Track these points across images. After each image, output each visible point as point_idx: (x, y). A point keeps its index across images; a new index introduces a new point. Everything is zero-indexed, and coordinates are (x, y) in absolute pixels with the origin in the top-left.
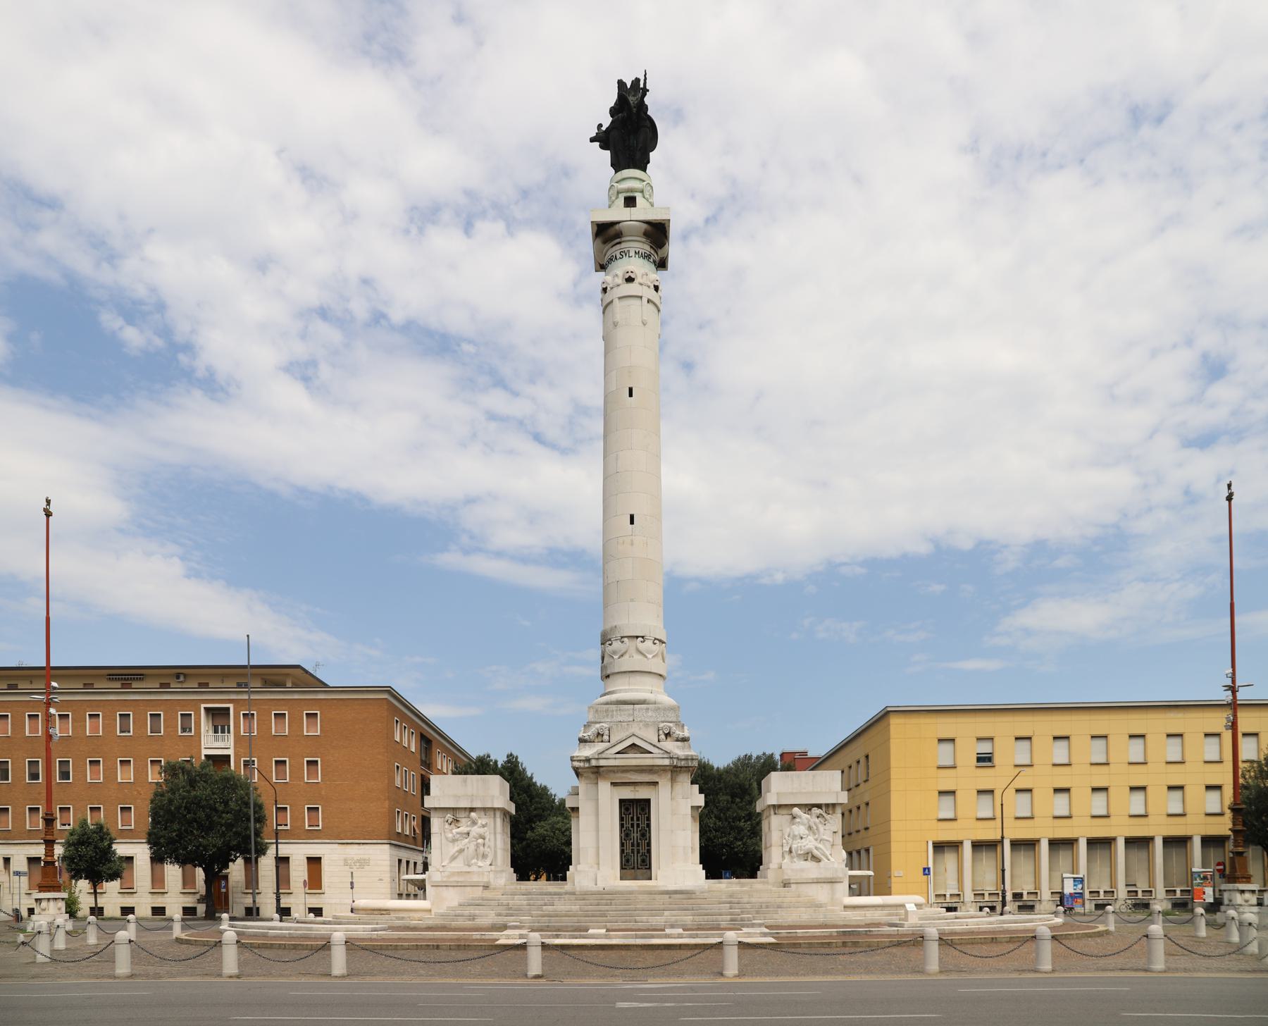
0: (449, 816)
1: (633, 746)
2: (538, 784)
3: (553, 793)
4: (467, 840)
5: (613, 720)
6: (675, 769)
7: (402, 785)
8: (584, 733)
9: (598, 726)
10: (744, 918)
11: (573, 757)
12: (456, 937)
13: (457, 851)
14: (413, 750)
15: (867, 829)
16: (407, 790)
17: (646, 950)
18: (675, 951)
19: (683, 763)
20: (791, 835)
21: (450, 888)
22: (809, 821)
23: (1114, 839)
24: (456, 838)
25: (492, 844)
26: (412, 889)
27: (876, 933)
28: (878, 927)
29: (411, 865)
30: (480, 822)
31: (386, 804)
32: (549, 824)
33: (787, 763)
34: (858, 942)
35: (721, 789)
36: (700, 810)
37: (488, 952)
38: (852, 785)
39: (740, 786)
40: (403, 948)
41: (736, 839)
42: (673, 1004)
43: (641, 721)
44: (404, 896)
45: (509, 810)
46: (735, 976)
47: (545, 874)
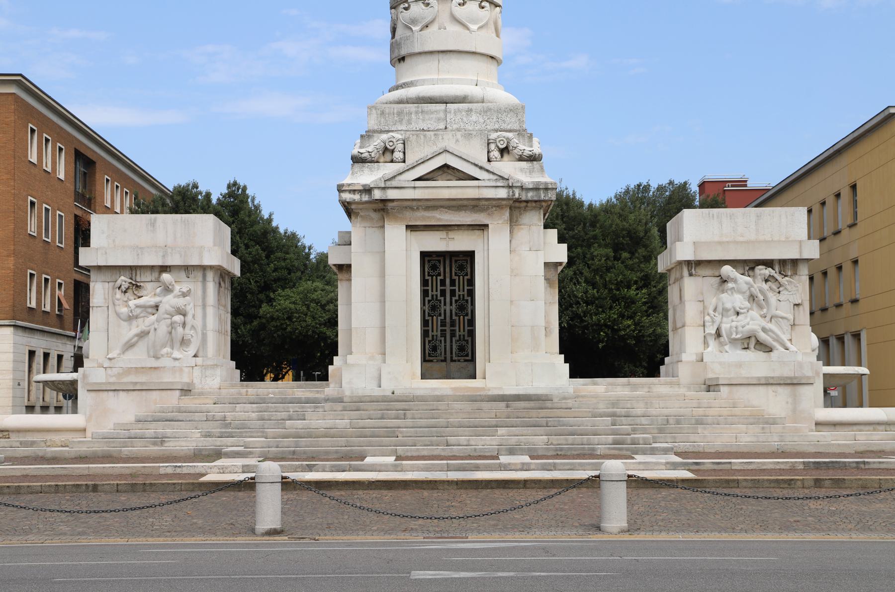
0: (123, 280)
1: (445, 169)
2: (282, 231)
3: (307, 245)
4: (153, 318)
5: (410, 127)
6: (517, 204)
7: (40, 233)
8: (361, 147)
9: (384, 137)
10: (638, 438)
11: (343, 185)
12: (128, 472)
13: (137, 335)
14: (62, 176)
15: (855, 301)
16: (49, 240)
17: (466, 488)
18: (515, 490)
19: (530, 195)
20: (720, 309)
21: (121, 393)
22: (750, 286)
24: (135, 314)
25: (198, 323)
26: (52, 397)
27: (875, 466)
28: (880, 457)
29: (53, 361)
30: (177, 288)
31: (11, 262)
32: (299, 294)
33: (711, 197)
34: (844, 479)
35: (595, 237)
36: (560, 268)
37: (185, 495)
38: (827, 232)
39: (629, 232)
40: (31, 491)
41: (622, 316)
42: (512, 574)
43: (458, 130)
44: (38, 409)
45: (229, 269)
46: (623, 531)
47: (290, 373)
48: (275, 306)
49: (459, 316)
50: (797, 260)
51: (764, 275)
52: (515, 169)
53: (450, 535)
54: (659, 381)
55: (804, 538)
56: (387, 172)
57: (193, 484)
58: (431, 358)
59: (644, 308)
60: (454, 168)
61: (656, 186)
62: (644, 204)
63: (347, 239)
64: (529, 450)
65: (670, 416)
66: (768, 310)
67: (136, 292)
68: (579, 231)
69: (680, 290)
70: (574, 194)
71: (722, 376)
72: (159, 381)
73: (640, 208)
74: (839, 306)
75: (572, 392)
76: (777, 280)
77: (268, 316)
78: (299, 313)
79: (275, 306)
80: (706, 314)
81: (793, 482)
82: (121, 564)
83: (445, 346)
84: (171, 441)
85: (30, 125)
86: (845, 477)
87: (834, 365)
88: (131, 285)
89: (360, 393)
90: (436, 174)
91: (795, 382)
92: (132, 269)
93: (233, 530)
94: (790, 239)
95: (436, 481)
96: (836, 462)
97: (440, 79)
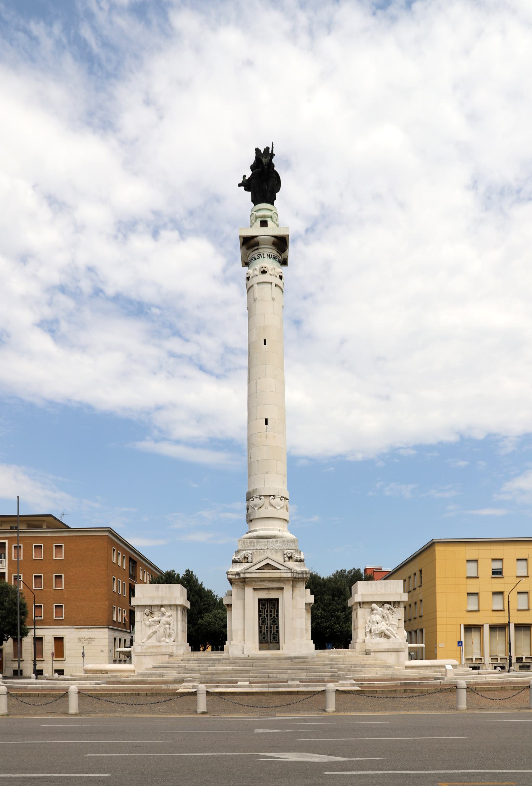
0: (147, 611)
1: (268, 565)
2: (206, 589)
3: (216, 595)
5: (254, 548)
6: (295, 579)
7: (117, 591)
8: (235, 556)
9: (244, 552)
10: (340, 674)
11: (229, 572)
12: (150, 688)
13: (152, 633)
14: (124, 568)
15: (421, 616)
17: (275, 695)
18: (294, 695)
19: (300, 576)
20: (371, 621)
22: (382, 612)
23: (483, 626)
25: (175, 628)
26: (122, 657)
28: (428, 680)
29: (123, 642)
30: (167, 614)
31: (107, 602)
32: (213, 615)
34: (415, 689)
35: (325, 591)
36: (311, 605)
38: (411, 589)
40: (116, 695)
41: (335, 623)
42: (292, 730)
43: (273, 549)
44: (118, 661)
45: (186, 606)
46: (334, 712)
47: (210, 647)
48: (204, 620)
49: (273, 625)
50: (399, 601)
51: (388, 607)
52: (294, 565)
53: (270, 714)
54: (348, 650)
55: (400, 713)
56: (245, 566)
57: (174, 693)
58: (262, 642)
59: (344, 620)
60: (271, 565)
61: (348, 570)
62: (343, 578)
63: (230, 594)
64: (299, 679)
65: (352, 665)
66: (389, 622)
67: (152, 616)
68: (319, 589)
69: (357, 614)
70: (317, 574)
71: (372, 648)
72: (161, 651)
73: (342, 579)
74: (415, 618)
75: (316, 655)
76: (392, 609)
77: (201, 624)
78: (213, 623)
79: (204, 620)
80: (366, 623)
81: (396, 691)
82: (149, 726)
83: (268, 637)
84: (165, 675)
85: (113, 548)
86: (415, 689)
87: (413, 643)
88: (150, 613)
89: (236, 656)
90: (264, 567)
91: (398, 650)
92: (150, 606)
93: (189, 712)
94: (397, 593)
95: (264, 692)
96: (412, 682)
97: (266, 529)
